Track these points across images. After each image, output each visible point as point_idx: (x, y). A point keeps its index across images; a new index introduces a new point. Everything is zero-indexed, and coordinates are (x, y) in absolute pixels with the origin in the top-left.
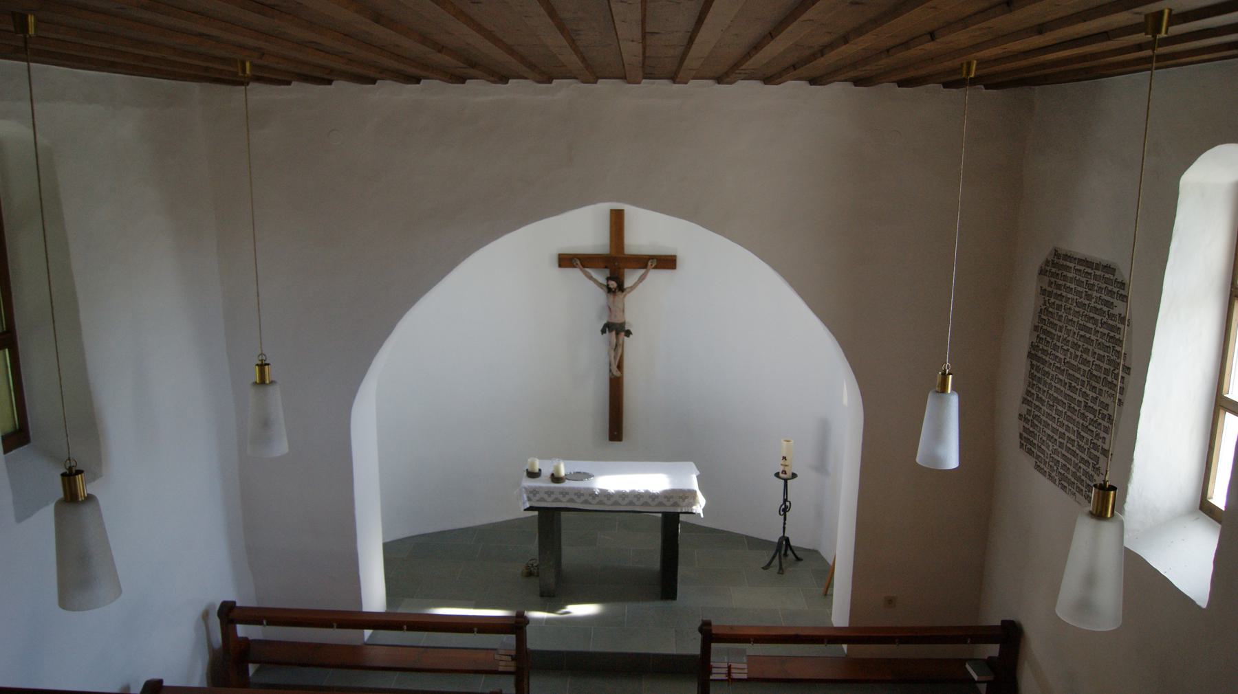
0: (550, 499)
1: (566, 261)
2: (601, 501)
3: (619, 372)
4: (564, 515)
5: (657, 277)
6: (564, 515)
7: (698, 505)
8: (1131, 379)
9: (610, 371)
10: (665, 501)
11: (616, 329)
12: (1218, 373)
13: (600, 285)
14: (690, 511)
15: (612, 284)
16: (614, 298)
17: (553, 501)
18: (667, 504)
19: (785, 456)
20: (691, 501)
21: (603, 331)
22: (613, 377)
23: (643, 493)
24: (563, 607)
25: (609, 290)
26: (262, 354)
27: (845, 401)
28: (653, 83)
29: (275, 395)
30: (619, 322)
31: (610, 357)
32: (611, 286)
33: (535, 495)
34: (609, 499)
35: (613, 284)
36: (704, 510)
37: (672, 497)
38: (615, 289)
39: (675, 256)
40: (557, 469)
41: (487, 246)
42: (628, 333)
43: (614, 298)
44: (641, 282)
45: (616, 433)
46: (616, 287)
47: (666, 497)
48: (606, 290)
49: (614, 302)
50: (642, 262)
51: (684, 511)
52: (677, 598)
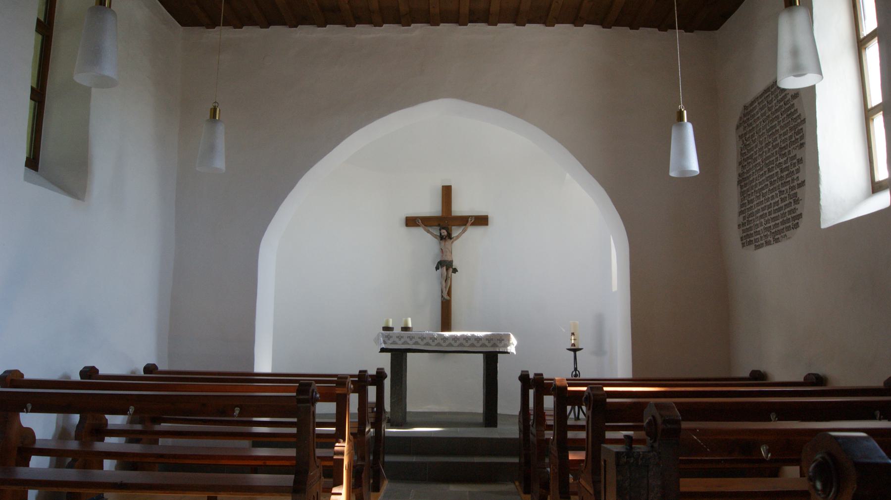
1: (411, 222)
2: (439, 343)
4: (409, 355)
5: (473, 233)
6: (409, 355)
8: (807, 127)
9: (442, 296)
11: (445, 265)
12: (859, 68)
13: (435, 236)
14: (506, 351)
17: (403, 344)
19: (573, 332)
21: (437, 268)
22: (444, 301)
25: (442, 238)
26: (215, 102)
27: (615, 287)
28: (476, 26)
29: (221, 129)
30: (450, 260)
31: (442, 285)
32: (443, 234)
33: (389, 339)
34: (444, 342)
35: (444, 233)
36: (517, 348)
37: (492, 339)
39: (487, 216)
40: (406, 322)
42: (455, 271)
44: (464, 233)
46: (446, 237)
47: (487, 339)
50: (464, 221)
51: (501, 350)
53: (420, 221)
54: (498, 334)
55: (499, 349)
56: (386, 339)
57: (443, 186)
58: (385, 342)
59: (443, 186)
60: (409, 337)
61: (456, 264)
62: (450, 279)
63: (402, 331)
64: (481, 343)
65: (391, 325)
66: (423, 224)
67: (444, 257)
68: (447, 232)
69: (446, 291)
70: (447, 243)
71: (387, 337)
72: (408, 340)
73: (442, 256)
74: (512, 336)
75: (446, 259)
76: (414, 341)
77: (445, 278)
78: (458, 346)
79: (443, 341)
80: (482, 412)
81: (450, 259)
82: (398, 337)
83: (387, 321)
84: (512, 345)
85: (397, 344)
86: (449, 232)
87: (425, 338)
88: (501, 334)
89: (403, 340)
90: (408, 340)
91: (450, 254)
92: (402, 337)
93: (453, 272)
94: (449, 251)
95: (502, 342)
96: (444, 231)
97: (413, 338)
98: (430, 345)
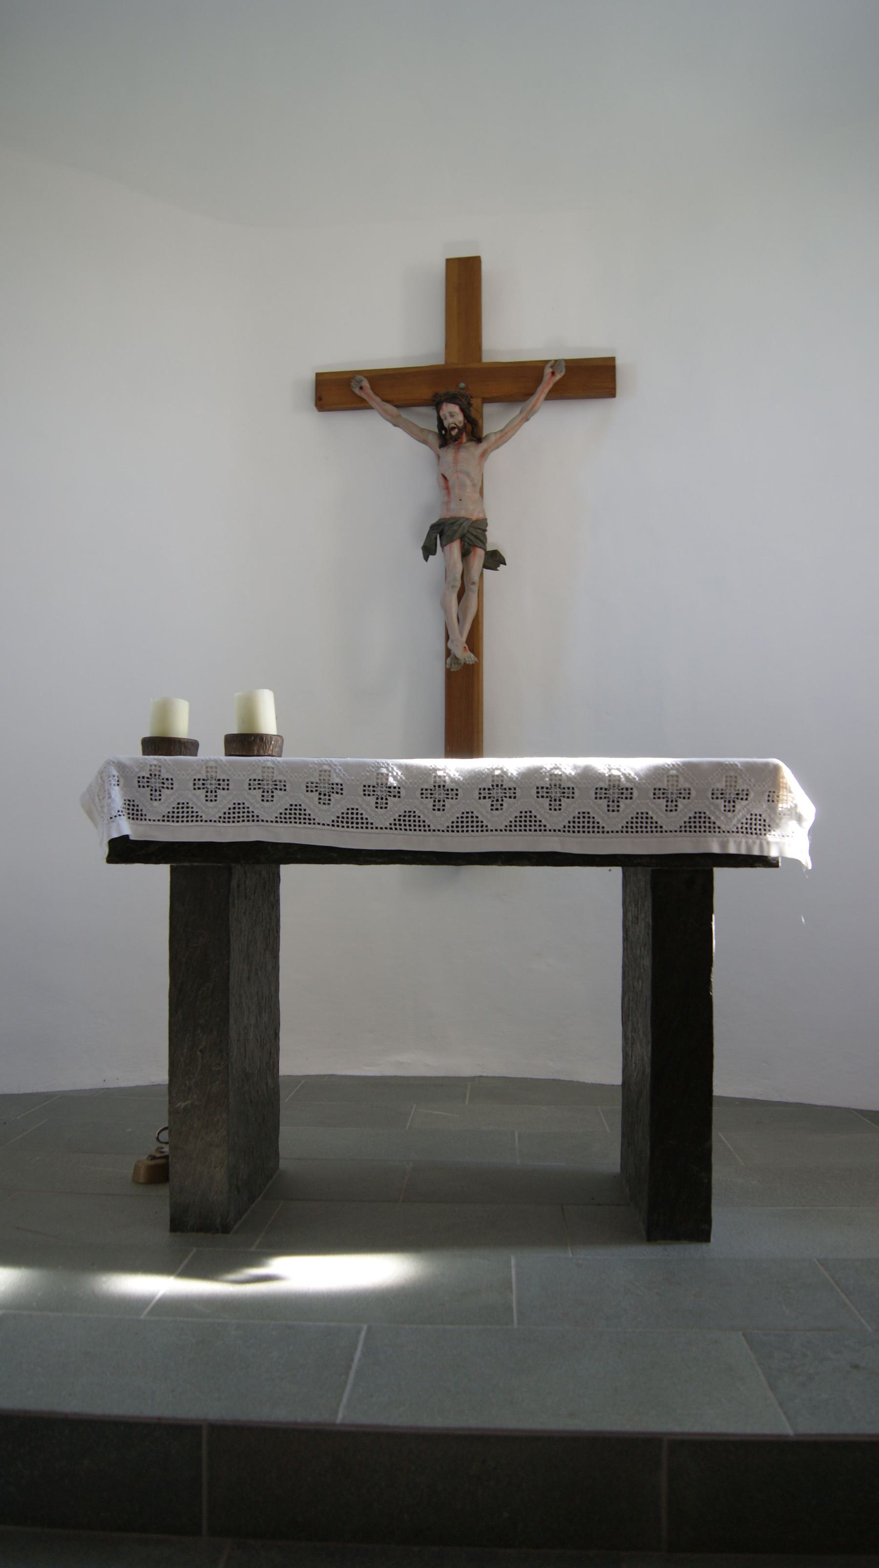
0: (213, 810)
3: (469, 654)
7: (791, 825)
9: (448, 652)
10: (657, 810)
13: (420, 435)
14: (756, 852)
18: (670, 821)
20: (761, 808)
21: (428, 550)
23: (569, 778)
24: (257, 1258)
33: (155, 794)
35: (453, 414)
37: (685, 794)
39: (613, 359)
40: (249, 711)
42: (495, 560)
44: (527, 419)
47: (659, 793)
49: (456, 461)
51: (732, 850)
52: (712, 1239)
53: (366, 384)
54: (720, 765)
55: (724, 845)
56: (143, 797)
57: (448, 261)
58: (134, 812)
59: (448, 261)
60: (256, 784)
61: (495, 539)
62: (475, 588)
63: (146, 752)
64: (628, 809)
65: (182, 729)
66: (377, 394)
67: (453, 505)
68: (467, 416)
69: (461, 633)
70: (463, 454)
71: (144, 782)
72: (253, 800)
73: (448, 503)
74: (788, 776)
75: (463, 514)
76: (282, 801)
77: (458, 584)
78: (510, 828)
79: (429, 803)
80: (615, 1077)
81: (481, 516)
82: (199, 784)
83: (164, 711)
84: (792, 824)
85: (195, 817)
86: (473, 414)
87: (338, 789)
88: (733, 766)
89: (225, 800)
90: (253, 800)
91: (477, 495)
92: (223, 784)
93: (485, 566)
94: (474, 485)
95: (739, 805)
96: (455, 409)
97: (279, 786)
98: (367, 825)
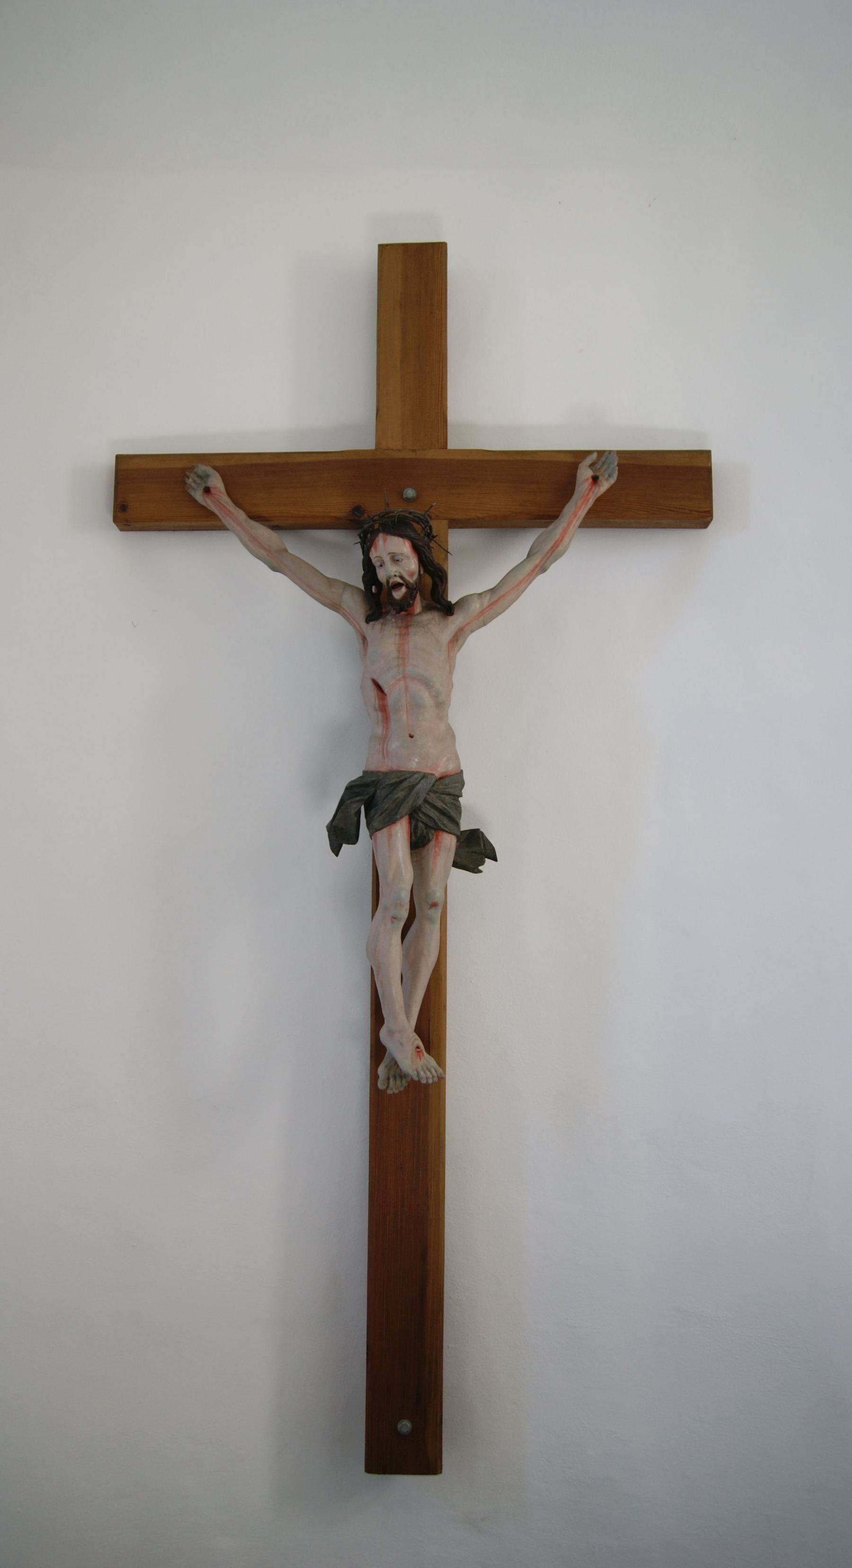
9: (378, 1051)
15: (395, 559)
16: (404, 635)
27: (400, 854)
32: (387, 572)
38: (412, 590)
39: (707, 454)
41: (371, 875)
43: (404, 635)
45: (405, 1426)
48: (356, 605)
49: (402, 655)
